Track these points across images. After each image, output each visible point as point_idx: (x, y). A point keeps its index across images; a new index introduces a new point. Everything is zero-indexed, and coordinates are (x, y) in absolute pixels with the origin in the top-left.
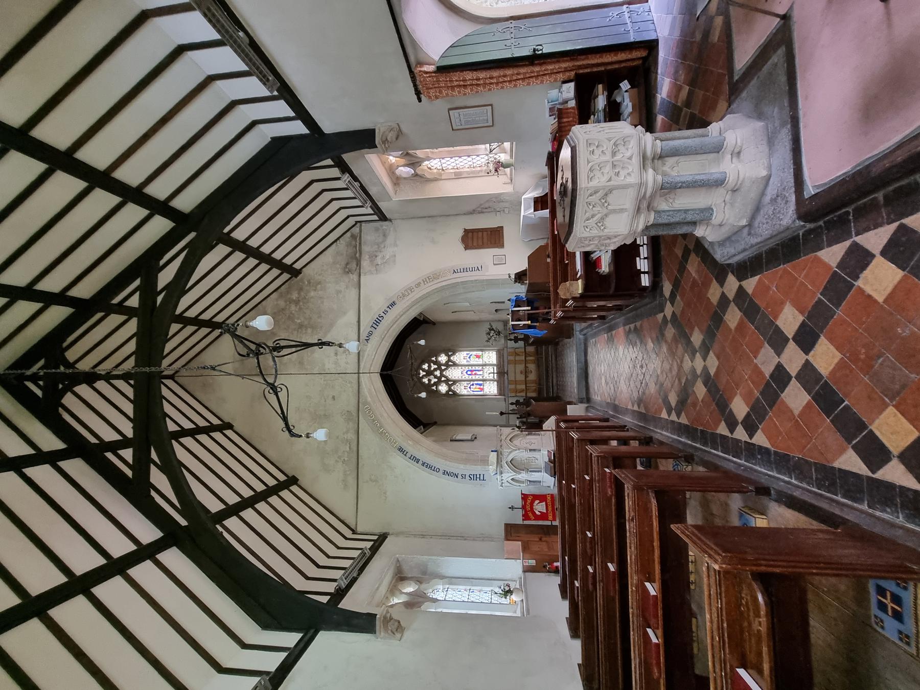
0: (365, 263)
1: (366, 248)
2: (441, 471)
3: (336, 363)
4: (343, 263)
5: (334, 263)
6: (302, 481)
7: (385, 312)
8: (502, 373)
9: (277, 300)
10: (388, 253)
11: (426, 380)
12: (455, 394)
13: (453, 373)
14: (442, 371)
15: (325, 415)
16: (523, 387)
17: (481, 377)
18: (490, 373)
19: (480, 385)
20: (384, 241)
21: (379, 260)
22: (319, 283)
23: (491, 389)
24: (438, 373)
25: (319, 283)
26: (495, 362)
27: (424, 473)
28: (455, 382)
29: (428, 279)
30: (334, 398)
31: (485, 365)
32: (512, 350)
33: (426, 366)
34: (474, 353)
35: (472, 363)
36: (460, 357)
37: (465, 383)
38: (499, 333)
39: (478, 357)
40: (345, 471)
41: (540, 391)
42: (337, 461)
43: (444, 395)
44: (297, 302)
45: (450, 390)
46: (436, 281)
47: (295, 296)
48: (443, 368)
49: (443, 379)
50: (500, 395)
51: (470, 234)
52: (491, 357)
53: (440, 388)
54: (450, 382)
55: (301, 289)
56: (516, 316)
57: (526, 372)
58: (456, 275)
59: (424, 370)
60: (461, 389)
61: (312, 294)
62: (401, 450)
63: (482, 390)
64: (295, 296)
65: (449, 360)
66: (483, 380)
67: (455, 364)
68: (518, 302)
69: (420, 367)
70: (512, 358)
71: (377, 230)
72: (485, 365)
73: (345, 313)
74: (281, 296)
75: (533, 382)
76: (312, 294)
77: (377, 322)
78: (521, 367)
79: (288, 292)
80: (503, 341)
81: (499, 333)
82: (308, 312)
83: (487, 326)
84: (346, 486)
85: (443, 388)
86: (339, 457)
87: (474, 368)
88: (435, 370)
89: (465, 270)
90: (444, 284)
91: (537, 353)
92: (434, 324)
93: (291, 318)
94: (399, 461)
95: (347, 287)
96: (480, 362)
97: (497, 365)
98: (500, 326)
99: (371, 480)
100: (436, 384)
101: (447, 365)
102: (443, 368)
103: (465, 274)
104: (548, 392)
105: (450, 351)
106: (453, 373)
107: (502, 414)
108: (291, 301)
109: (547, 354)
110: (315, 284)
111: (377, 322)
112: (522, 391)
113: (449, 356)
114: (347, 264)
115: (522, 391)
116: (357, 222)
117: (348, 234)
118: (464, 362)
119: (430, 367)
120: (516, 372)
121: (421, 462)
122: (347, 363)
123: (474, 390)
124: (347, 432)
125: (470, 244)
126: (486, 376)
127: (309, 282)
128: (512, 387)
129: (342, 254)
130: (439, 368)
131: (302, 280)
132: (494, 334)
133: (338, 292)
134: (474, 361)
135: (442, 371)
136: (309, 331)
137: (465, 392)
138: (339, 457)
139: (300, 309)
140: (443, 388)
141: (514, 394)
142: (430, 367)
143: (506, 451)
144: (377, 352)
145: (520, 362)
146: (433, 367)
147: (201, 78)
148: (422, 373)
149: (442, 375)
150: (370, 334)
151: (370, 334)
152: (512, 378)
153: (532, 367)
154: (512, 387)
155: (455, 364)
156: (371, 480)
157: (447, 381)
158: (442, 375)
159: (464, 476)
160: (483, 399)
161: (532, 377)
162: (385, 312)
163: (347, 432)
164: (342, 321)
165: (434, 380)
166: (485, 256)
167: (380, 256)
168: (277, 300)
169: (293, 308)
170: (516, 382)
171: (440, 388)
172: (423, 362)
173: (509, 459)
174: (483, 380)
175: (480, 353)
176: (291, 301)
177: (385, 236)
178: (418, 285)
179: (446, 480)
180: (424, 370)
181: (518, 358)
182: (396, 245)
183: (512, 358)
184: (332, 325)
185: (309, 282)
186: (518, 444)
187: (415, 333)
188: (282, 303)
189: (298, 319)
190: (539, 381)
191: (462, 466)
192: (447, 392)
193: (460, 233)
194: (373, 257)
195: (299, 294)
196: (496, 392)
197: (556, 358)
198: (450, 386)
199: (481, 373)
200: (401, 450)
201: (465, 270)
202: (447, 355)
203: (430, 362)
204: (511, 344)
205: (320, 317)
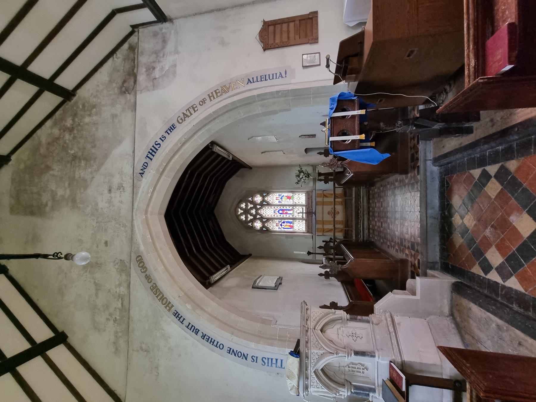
0: (142, 78)
1: (143, 60)
2: (226, 349)
3: (110, 202)
4: (120, 81)
5: (111, 82)
6: (73, 340)
7: (163, 138)
8: (310, 213)
9: (52, 128)
10: (167, 63)
11: (243, 217)
12: (268, 230)
13: (267, 212)
14: (257, 210)
15: (97, 263)
16: (331, 227)
17: (291, 216)
18: (299, 212)
19: (290, 223)
20: (164, 47)
21: (157, 74)
22: (94, 107)
23: (300, 227)
24: (253, 212)
25: (94, 107)
26: (304, 203)
27: (204, 350)
28: (268, 220)
29: (213, 95)
30: (106, 243)
31: (295, 205)
32: (321, 192)
33: (243, 205)
34: (286, 194)
35: (283, 203)
36: (273, 198)
37: (277, 221)
38: (308, 175)
39: (289, 198)
40: (116, 332)
41: (347, 234)
42: (108, 319)
43: (258, 231)
44: (71, 130)
45: (264, 226)
46: (225, 96)
47: (69, 122)
48: (258, 207)
49: (258, 216)
50: (308, 232)
51: (271, 28)
52: (301, 198)
53: (255, 224)
54: (265, 220)
55: (75, 115)
56: (336, 126)
57: (334, 213)
58: (251, 86)
59: (242, 209)
60: (273, 226)
61: (87, 120)
62: (177, 315)
63: (292, 227)
64: (69, 122)
65: (263, 201)
66: (293, 219)
67: (268, 204)
68: (342, 103)
69: (238, 206)
70: (319, 199)
71: (155, 34)
72: (295, 205)
73: (120, 142)
74: (55, 124)
75: (340, 222)
76: (87, 120)
77: (152, 152)
78: (328, 208)
79: (63, 119)
80: (311, 184)
81: (308, 175)
82: (82, 141)
83: (295, 171)
84: (117, 351)
85: (258, 225)
86: (111, 315)
87: (285, 208)
88: (251, 208)
89: (264, 78)
90: (235, 98)
91: (345, 194)
92: (250, 168)
93: (65, 148)
94: (173, 328)
95: (123, 110)
96: (291, 202)
97: (306, 206)
98: (310, 170)
99: (142, 349)
100: (252, 221)
101: (262, 204)
102: (258, 207)
103: (264, 83)
104: (357, 235)
105: (264, 192)
106: (267, 212)
107: (309, 253)
108: (65, 129)
109: (358, 196)
110: (91, 108)
111: (152, 152)
112: (330, 231)
113: (263, 197)
114: (124, 82)
115: (330, 231)
116: (135, 27)
117: (126, 46)
118: (277, 202)
119: (247, 206)
120: (324, 213)
121: (200, 334)
122: (121, 202)
123: (286, 228)
124: (120, 285)
125: (271, 41)
126: (296, 215)
127: (84, 106)
128: (320, 226)
129: (118, 71)
130: (255, 207)
131: (76, 103)
132: (303, 174)
133: (114, 116)
134: (285, 201)
135: (257, 210)
136: (83, 163)
137: (277, 229)
138: (111, 315)
139: (74, 138)
140: (258, 225)
141: (321, 234)
142: (247, 206)
143: (314, 352)
144: (158, 188)
145: (329, 203)
146: (250, 206)
147: (109, 11)
148: (240, 211)
149: (257, 213)
150: (145, 166)
151: (145, 166)
152: (319, 217)
153: (339, 208)
154: (320, 226)
155: (268, 204)
156: (142, 349)
157: (261, 219)
158: (257, 213)
159: (254, 359)
160: (292, 235)
161: (340, 217)
162: (163, 138)
163: (120, 285)
164: (117, 151)
165: (250, 217)
166: (294, 55)
167: (158, 67)
168: (52, 128)
169: (67, 136)
170: (323, 222)
171: (255, 224)
172: (241, 202)
173: (321, 365)
174: (293, 219)
175: (290, 194)
176: (65, 129)
177: (164, 42)
178: (203, 102)
179: (231, 361)
180: (242, 209)
181: (326, 199)
182: (177, 52)
183: (319, 199)
184: (106, 156)
185: (84, 106)
186: (334, 337)
187: (234, 177)
188: (56, 132)
189: (72, 149)
190: (347, 223)
191: (253, 345)
192: (262, 228)
193: (258, 27)
194: (150, 69)
195: (73, 120)
196: (304, 229)
197: (369, 199)
198: (263, 223)
199: (291, 212)
200: (177, 315)
201: (264, 78)
202: (262, 195)
203: (247, 202)
204: (321, 185)
205: (94, 147)
